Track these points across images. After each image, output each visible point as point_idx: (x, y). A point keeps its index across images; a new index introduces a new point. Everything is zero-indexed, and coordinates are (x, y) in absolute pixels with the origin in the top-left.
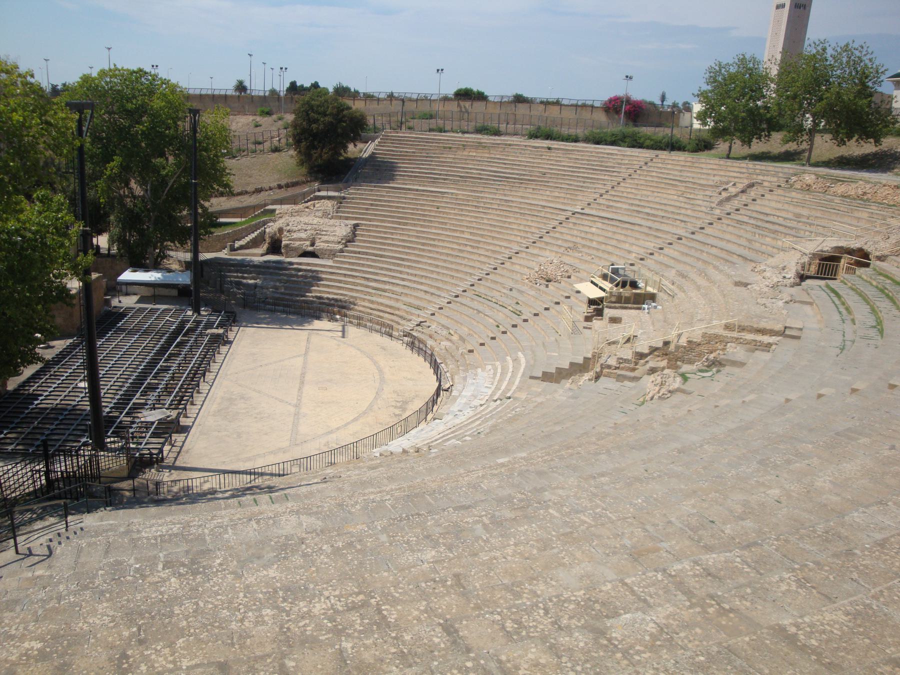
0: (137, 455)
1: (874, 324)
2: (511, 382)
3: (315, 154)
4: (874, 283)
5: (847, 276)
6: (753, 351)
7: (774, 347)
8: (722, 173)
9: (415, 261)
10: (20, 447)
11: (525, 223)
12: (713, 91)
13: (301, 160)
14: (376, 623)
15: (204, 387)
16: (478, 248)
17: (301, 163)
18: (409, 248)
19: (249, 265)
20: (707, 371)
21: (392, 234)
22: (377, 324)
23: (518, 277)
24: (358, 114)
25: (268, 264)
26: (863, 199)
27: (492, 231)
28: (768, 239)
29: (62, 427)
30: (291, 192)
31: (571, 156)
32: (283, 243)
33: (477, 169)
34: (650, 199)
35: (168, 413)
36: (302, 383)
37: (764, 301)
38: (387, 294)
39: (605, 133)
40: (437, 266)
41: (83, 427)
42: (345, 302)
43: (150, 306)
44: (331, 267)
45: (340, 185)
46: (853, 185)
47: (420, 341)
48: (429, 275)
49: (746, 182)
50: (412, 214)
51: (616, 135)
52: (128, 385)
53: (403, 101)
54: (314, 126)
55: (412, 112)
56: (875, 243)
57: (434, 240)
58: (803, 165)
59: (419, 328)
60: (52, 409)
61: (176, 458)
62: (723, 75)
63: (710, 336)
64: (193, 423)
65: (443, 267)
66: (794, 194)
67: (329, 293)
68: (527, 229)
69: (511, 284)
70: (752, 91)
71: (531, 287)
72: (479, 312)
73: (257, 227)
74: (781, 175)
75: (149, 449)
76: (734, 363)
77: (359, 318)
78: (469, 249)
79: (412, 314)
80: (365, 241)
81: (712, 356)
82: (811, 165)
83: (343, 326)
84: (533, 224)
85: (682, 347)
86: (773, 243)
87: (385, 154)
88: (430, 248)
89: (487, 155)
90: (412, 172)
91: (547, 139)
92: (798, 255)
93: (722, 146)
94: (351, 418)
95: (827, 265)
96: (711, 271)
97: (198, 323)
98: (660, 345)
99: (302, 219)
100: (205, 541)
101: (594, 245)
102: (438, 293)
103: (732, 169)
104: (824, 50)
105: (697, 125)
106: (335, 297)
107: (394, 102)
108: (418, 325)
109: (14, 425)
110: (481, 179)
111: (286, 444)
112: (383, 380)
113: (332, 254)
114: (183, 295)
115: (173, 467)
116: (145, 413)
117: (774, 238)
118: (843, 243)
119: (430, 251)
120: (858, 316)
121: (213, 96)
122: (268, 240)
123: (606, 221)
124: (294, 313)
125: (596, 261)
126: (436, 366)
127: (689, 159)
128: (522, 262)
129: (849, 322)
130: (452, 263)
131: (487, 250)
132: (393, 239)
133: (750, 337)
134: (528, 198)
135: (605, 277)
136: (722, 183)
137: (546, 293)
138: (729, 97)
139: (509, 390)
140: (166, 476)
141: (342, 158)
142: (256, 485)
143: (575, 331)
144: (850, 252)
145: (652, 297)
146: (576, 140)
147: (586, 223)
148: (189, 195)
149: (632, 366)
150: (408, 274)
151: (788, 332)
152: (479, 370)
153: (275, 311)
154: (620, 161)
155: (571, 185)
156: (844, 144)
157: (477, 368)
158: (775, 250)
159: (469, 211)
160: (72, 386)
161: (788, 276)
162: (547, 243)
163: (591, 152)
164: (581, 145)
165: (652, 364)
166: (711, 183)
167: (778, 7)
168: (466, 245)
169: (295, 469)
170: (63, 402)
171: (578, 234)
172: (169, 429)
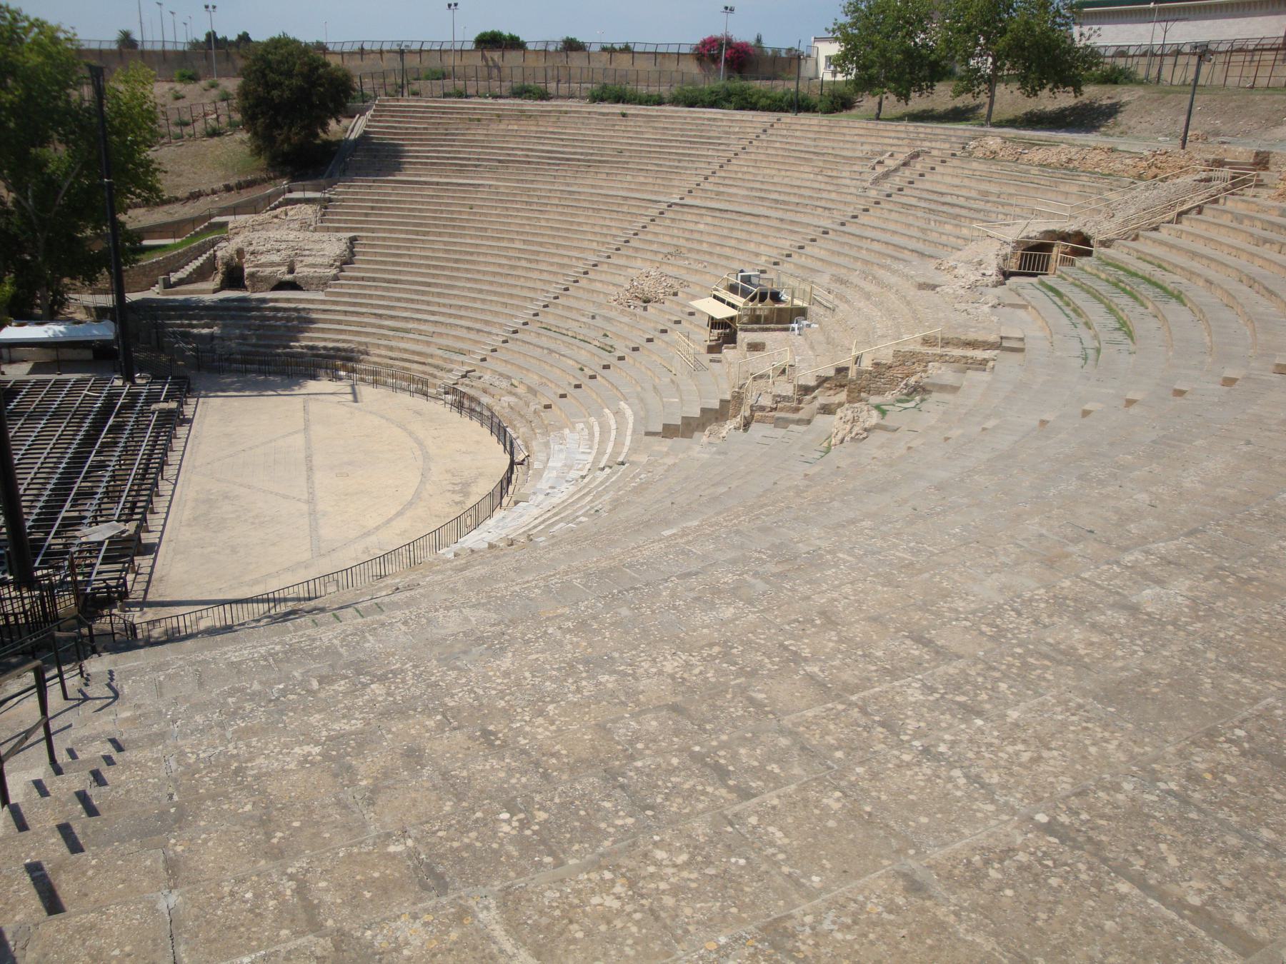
0: (89, 590)
1: (1118, 326)
2: (618, 443)
3: (280, 135)
4: (1103, 276)
5: (1064, 269)
7: (991, 364)
8: (873, 140)
9: (447, 286)
12: (855, 23)
13: (258, 147)
14: (788, 660)
15: (164, 487)
16: (537, 261)
17: (258, 152)
18: (435, 267)
19: (197, 307)
20: (908, 401)
21: (408, 248)
22: (403, 378)
23: (601, 299)
24: (340, 73)
25: (226, 304)
26: (1068, 168)
27: (554, 237)
30: (245, 195)
31: (656, 125)
32: (247, 271)
33: (522, 150)
34: (775, 180)
35: (122, 526)
36: (310, 469)
37: (963, 306)
38: (411, 336)
39: (702, 90)
40: (481, 291)
42: (352, 351)
45: (322, 182)
46: (1054, 150)
47: (472, 399)
48: (470, 305)
49: (909, 151)
50: (435, 218)
51: (717, 93)
52: (48, 492)
53: (402, 52)
54: (275, 93)
55: (415, 70)
56: (1097, 223)
57: (472, 254)
58: (982, 125)
59: (466, 381)
61: (146, 591)
64: (161, 538)
65: (488, 292)
66: (975, 165)
67: (325, 340)
68: (605, 231)
69: (592, 309)
71: (622, 311)
72: (551, 351)
73: (200, 250)
74: (954, 139)
75: (104, 581)
76: (943, 388)
77: (375, 373)
78: (524, 263)
79: (452, 361)
80: (369, 262)
81: (912, 381)
82: (993, 125)
83: (353, 386)
84: (612, 224)
85: (866, 372)
86: (957, 232)
87: (384, 133)
89: (534, 128)
90: (427, 158)
91: (618, 102)
92: (997, 245)
93: (868, 103)
94: (393, 512)
95: (1032, 257)
96: (881, 273)
97: (134, 397)
100: (341, 655)
101: (705, 247)
102: (487, 329)
103: (886, 134)
107: (386, 56)
108: (464, 376)
110: (529, 163)
111: (306, 556)
112: (427, 457)
113: (322, 283)
114: (100, 357)
115: (144, 604)
116: (85, 530)
117: (956, 225)
118: (1055, 226)
119: (467, 270)
122: (221, 268)
123: (718, 214)
124: (275, 373)
125: (711, 269)
126: (500, 431)
127: (825, 123)
128: (603, 277)
130: (501, 285)
131: (552, 264)
132: (410, 256)
134: (601, 187)
135: (733, 289)
136: (874, 154)
137: (645, 319)
139: (619, 454)
140: (136, 616)
141: (318, 142)
142: (285, 610)
143: (698, 367)
144: (1064, 237)
145: (802, 312)
146: (659, 102)
147: (689, 218)
148: (101, 206)
149: (794, 404)
150: (439, 304)
151: (1005, 344)
152: (567, 431)
153: (247, 371)
155: (661, 165)
156: (1036, 95)
157: (561, 428)
158: (960, 242)
159: (518, 210)
162: (636, 249)
164: (668, 109)
165: (822, 400)
168: (519, 258)
171: (680, 234)
172: (128, 549)
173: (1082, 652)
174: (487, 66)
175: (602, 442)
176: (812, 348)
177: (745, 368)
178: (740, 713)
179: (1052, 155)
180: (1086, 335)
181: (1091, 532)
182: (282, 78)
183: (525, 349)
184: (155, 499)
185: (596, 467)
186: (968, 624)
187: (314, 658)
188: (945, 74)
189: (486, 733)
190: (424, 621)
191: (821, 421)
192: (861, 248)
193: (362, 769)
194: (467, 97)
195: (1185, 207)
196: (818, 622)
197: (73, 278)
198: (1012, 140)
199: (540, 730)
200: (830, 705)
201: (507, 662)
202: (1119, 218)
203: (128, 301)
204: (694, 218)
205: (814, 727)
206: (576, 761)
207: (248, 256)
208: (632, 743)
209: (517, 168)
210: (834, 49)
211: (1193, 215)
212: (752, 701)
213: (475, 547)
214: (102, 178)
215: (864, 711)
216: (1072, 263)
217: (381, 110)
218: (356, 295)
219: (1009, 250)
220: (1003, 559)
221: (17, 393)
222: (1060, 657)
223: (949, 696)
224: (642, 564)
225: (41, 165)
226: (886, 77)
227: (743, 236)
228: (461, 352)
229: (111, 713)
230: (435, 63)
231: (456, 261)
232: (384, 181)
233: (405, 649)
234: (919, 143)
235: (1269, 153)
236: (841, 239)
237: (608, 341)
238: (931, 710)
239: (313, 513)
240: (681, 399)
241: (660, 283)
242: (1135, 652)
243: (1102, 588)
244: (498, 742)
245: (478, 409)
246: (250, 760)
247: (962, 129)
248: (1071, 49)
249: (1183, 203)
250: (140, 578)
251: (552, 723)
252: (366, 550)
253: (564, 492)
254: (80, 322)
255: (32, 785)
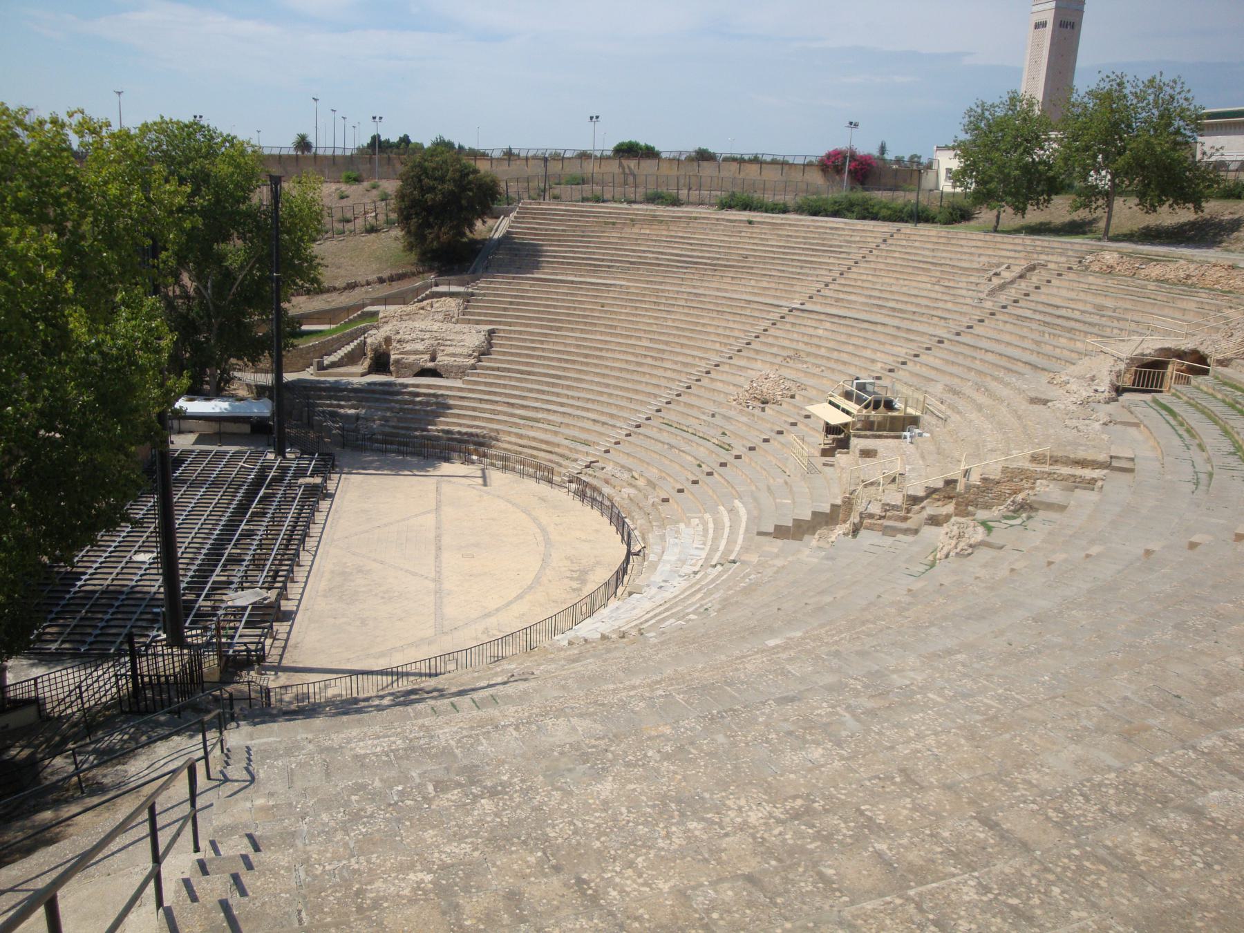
0: (231, 652)
1: (1232, 450)
3: (430, 234)
4: (1219, 396)
5: (1179, 387)
6: (1072, 490)
7: (1099, 483)
8: (990, 252)
10: (67, 646)
11: (724, 324)
13: (410, 243)
14: (864, 827)
15: (305, 558)
16: (662, 359)
17: (410, 247)
18: (567, 361)
19: (346, 389)
20: (1014, 518)
22: (530, 465)
23: (721, 398)
24: (488, 179)
26: (1186, 285)
27: (679, 336)
28: (1062, 340)
29: (120, 616)
30: (397, 287)
32: (393, 357)
33: (653, 252)
35: (264, 593)
36: (439, 549)
37: (1074, 423)
38: (540, 425)
39: (826, 200)
40: (608, 386)
41: (149, 616)
42: (484, 437)
43: (215, 448)
44: (460, 389)
45: (466, 277)
46: (1172, 266)
47: (594, 489)
49: (1025, 264)
50: (568, 315)
52: (202, 557)
53: (545, 160)
54: (429, 196)
55: (561, 175)
57: (601, 349)
58: (1100, 239)
59: (590, 471)
60: (103, 592)
61: (282, 656)
62: (988, 120)
63: (1013, 471)
64: (298, 606)
65: (616, 387)
66: (1091, 279)
67: (460, 425)
68: (728, 333)
69: (712, 408)
70: (1027, 140)
71: (741, 411)
72: (671, 446)
74: (1070, 253)
75: (245, 644)
76: (1050, 506)
79: (577, 451)
80: (505, 353)
81: (1019, 498)
83: (483, 470)
84: (735, 326)
85: (975, 486)
86: (1071, 345)
87: (525, 234)
88: (595, 361)
89: (665, 233)
90: (564, 257)
91: (745, 209)
92: (1111, 361)
93: (986, 215)
94: (514, 595)
95: (1148, 374)
97: (284, 470)
98: (940, 484)
99: (416, 324)
100: (455, 756)
101: (823, 352)
102: (612, 422)
104: (1120, 84)
105: (946, 186)
106: (469, 430)
108: (587, 467)
109: (53, 616)
110: (659, 265)
112: (548, 543)
113: (460, 372)
114: (259, 431)
115: (279, 668)
116: (232, 594)
117: (1071, 339)
118: (1170, 343)
119: (596, 365)
120: (1207, 440)
121: (280, 156)
122: (370, 354)
123: (836, 320)
124: (412, 454)
125: (827, 373)
126: (619, 522)
127: (943, 234)
128: (724, 377)
129: (1194, 448)
130: (627, 380)
131: (676, 363)
133: (1066, 470)
134: (726, 291)
135: (848, 395)
136: (991, 265)
138: (998, 150)
139: (732, 552)
140: (272, 681)
141: (465, 240)
142: (410, 692)
143: (811, 470)
144: (1180, 355)
145: (914, 421)
146: (785, 210)
147: (809, 323)
149: (903, 514)
151: (1115, 463)
152: (682, 526)
153: (386, 451)
157: (677, 522)
158: (1074, 355)
159: (646, 310)
160: (125, 560)
161: (1101, 389)
162: (757, 352)
163: (808, 227)
164: (792, 217)
166: (976, 266)
167: (1037, 26)
169: (452, 666)
170: (116, 582)
172: (269, 615)
173: (1139, 858)
174: (624, 173)
175: (715, 539)
176: (923, 457)
177: (856, 474)
178: (810, 888)
179: (1170, 271)
180: (1199, 457)
181: (1178, 697)
182: (436, 183)
183: (647, 443)
184: (295, 568)
185: (708, 564)
186: (1035, 807)
187: (432, 757)
188: (1063, 188)
189: (580, 881)
190: (534, 727)
191: (929, 531)
193: (468, 909)
194: (604, 201)
196: (898, 780)
197: (240, 358)
198: (1129, 255)
199: (629, 882)
200: (888, 899)
201: (606, 788)
203: (285, 380)
204: (813, 324)
205: (871, 921)
206: (657, 927)
207: (394, 344)
208: (708, 911)
209: (647, 270)
210: (955, 164)
212: (821, 876)
213: (589, 636)
214: (271, 272)
215: (919, 908)
216: (1188, 382)
217: (524, 212)
218: (491, 384)
219: (1122, 366)
220: (1085, 722)
221: (183, 462)
222: (1116, 862)
223: (1002, 898)
224: (743, 683)
225: (221, 258)
226: (1004, 192)
227: (861, 342)
228: (586, 443)
229: (247, 799)
230: (574, 169)
231: (586, 356)
232: (523, 279)
233: (515, 757)
234: (1035, 256)
236: (956, 349)
237: (726, 439)
238: (983, 912)
239: (438, 592)
240: (794, 503)
241: (779, 385)
242: (1194, 862)
243: (1174, 775)
244: (590, 892)
245: (600, 499)
246: (370, 883)
247: (1078, 243)
248: (1195, 166)
250: (277, 643)
251: (640, 876)
252: (486, 631)
253: (677, 586)
254: (242, 399)
255: (181, 883)
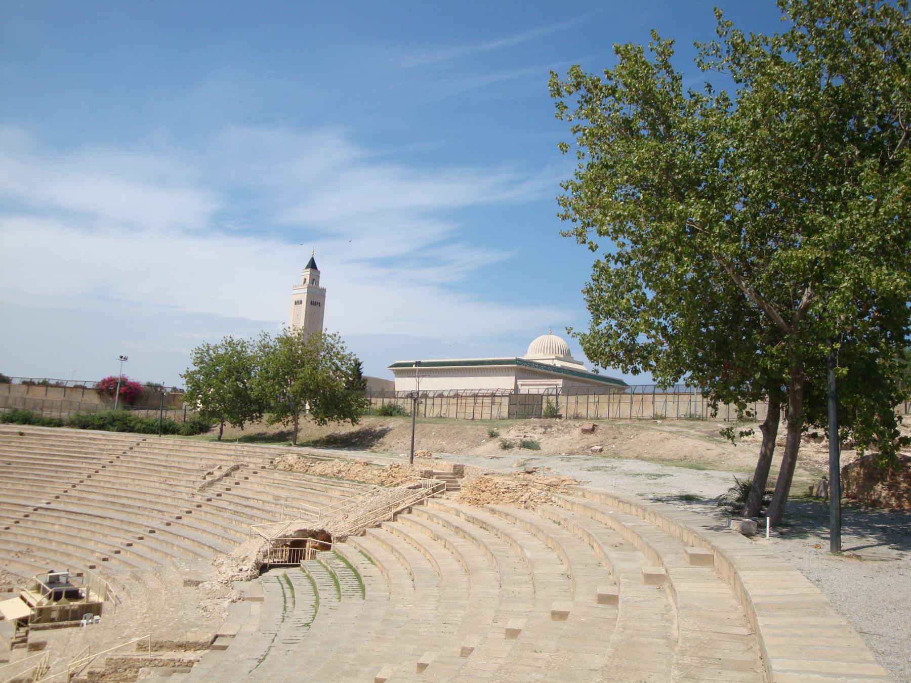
6: (169, 674)
7: (195, 665)
8: (210, 456)
31: (47, 442)
34: (129, 488)
46: (330, 464)
49: (232, 464)
58: (290, 445)
74: (267, 456)
91: (24, 423)
92: (262, 541)
101: (54, 546)
118: (307, 526)
127: (178, 443)
144: (314, 534)
145: (95, 609)
146: (60, 424)
147: (50, 520)
154: (103, 447)
156: (325, 423)
161: (245, 568)
163: (71, 437)
166: (197, 467)
171: (37, 534)
192: (173, 544)
195: (399, 509)
202: (351, 519)
211: (405, 515)
235: (463, 466)
249: (398, 505)
